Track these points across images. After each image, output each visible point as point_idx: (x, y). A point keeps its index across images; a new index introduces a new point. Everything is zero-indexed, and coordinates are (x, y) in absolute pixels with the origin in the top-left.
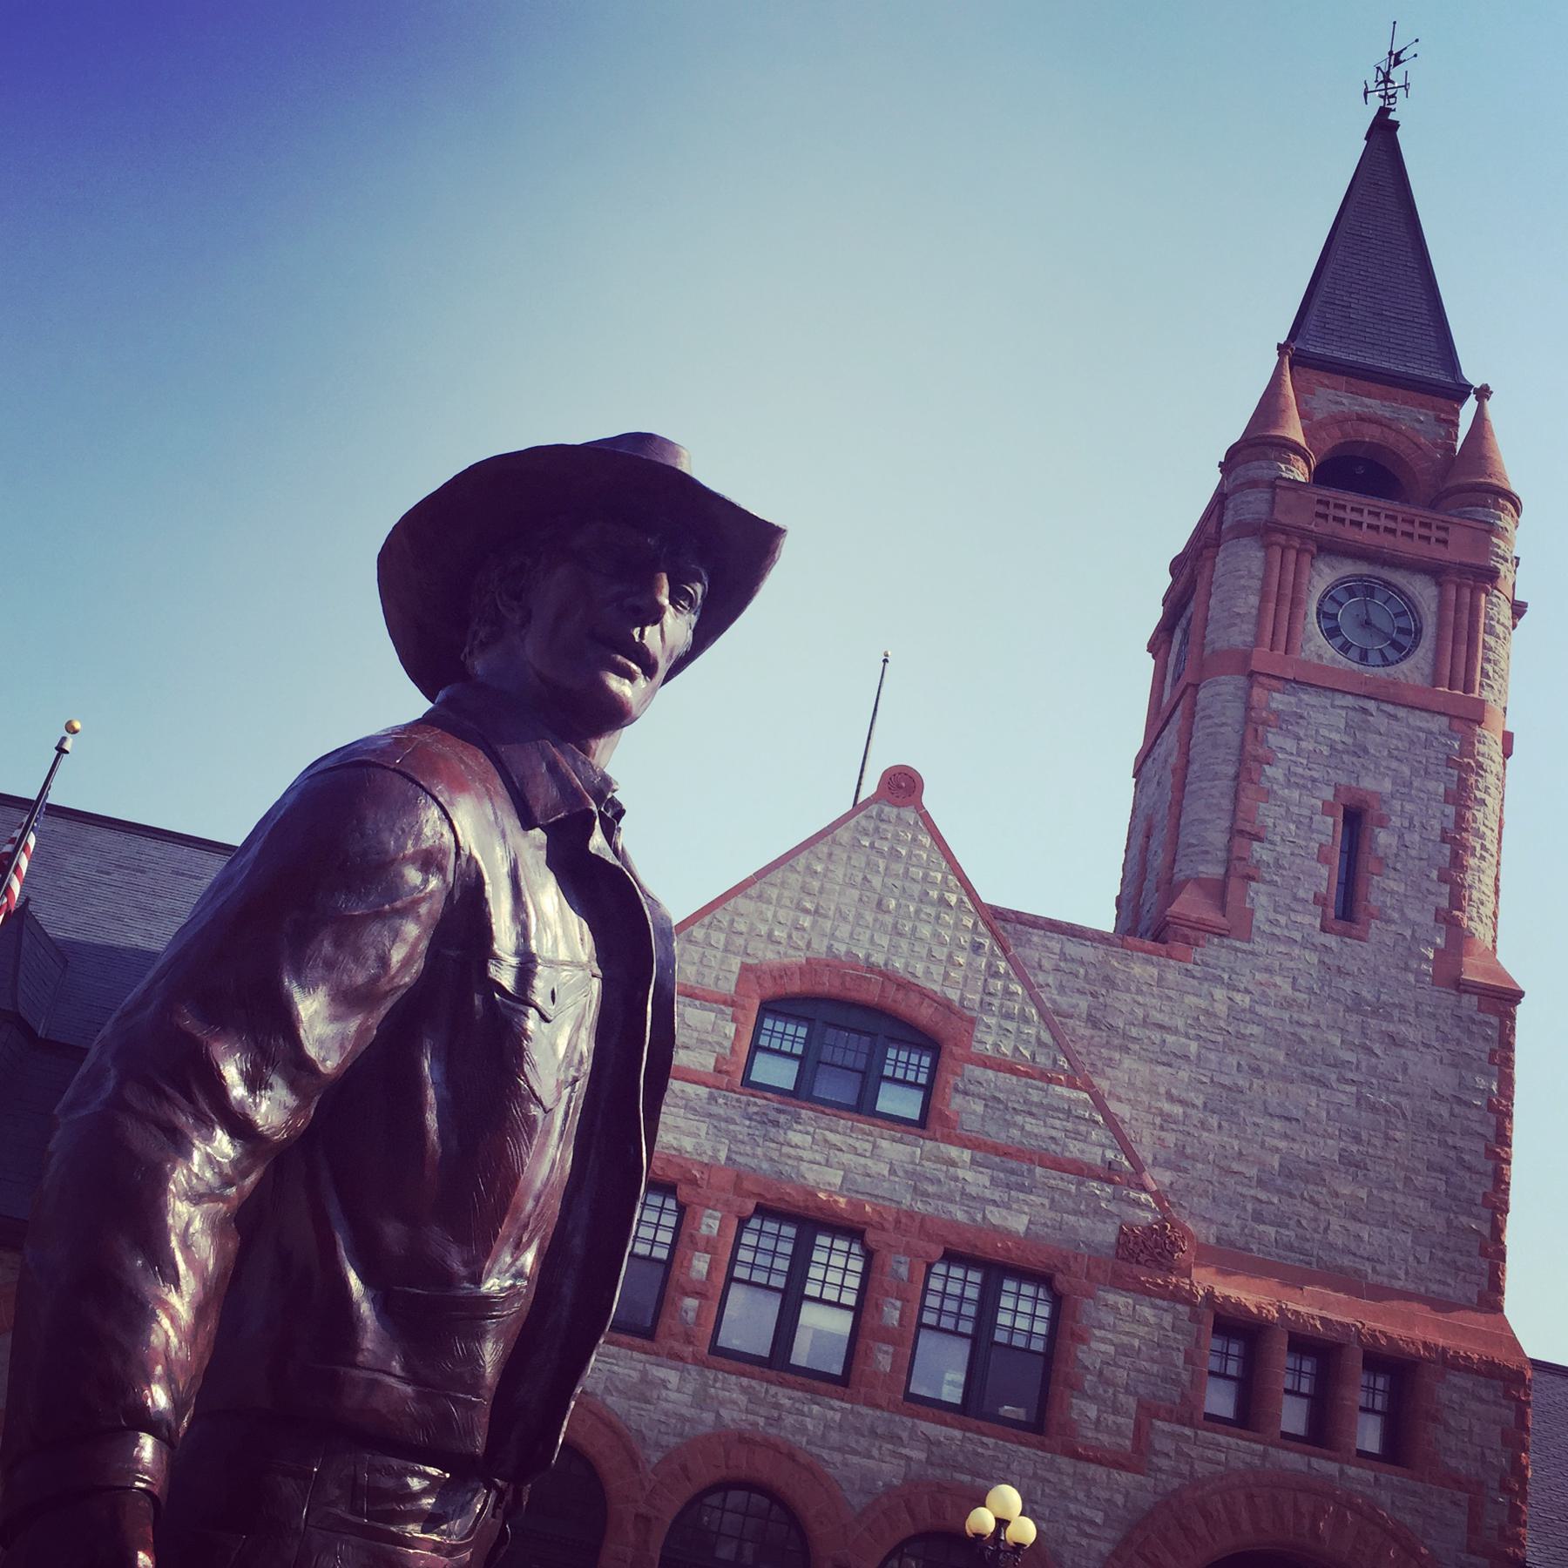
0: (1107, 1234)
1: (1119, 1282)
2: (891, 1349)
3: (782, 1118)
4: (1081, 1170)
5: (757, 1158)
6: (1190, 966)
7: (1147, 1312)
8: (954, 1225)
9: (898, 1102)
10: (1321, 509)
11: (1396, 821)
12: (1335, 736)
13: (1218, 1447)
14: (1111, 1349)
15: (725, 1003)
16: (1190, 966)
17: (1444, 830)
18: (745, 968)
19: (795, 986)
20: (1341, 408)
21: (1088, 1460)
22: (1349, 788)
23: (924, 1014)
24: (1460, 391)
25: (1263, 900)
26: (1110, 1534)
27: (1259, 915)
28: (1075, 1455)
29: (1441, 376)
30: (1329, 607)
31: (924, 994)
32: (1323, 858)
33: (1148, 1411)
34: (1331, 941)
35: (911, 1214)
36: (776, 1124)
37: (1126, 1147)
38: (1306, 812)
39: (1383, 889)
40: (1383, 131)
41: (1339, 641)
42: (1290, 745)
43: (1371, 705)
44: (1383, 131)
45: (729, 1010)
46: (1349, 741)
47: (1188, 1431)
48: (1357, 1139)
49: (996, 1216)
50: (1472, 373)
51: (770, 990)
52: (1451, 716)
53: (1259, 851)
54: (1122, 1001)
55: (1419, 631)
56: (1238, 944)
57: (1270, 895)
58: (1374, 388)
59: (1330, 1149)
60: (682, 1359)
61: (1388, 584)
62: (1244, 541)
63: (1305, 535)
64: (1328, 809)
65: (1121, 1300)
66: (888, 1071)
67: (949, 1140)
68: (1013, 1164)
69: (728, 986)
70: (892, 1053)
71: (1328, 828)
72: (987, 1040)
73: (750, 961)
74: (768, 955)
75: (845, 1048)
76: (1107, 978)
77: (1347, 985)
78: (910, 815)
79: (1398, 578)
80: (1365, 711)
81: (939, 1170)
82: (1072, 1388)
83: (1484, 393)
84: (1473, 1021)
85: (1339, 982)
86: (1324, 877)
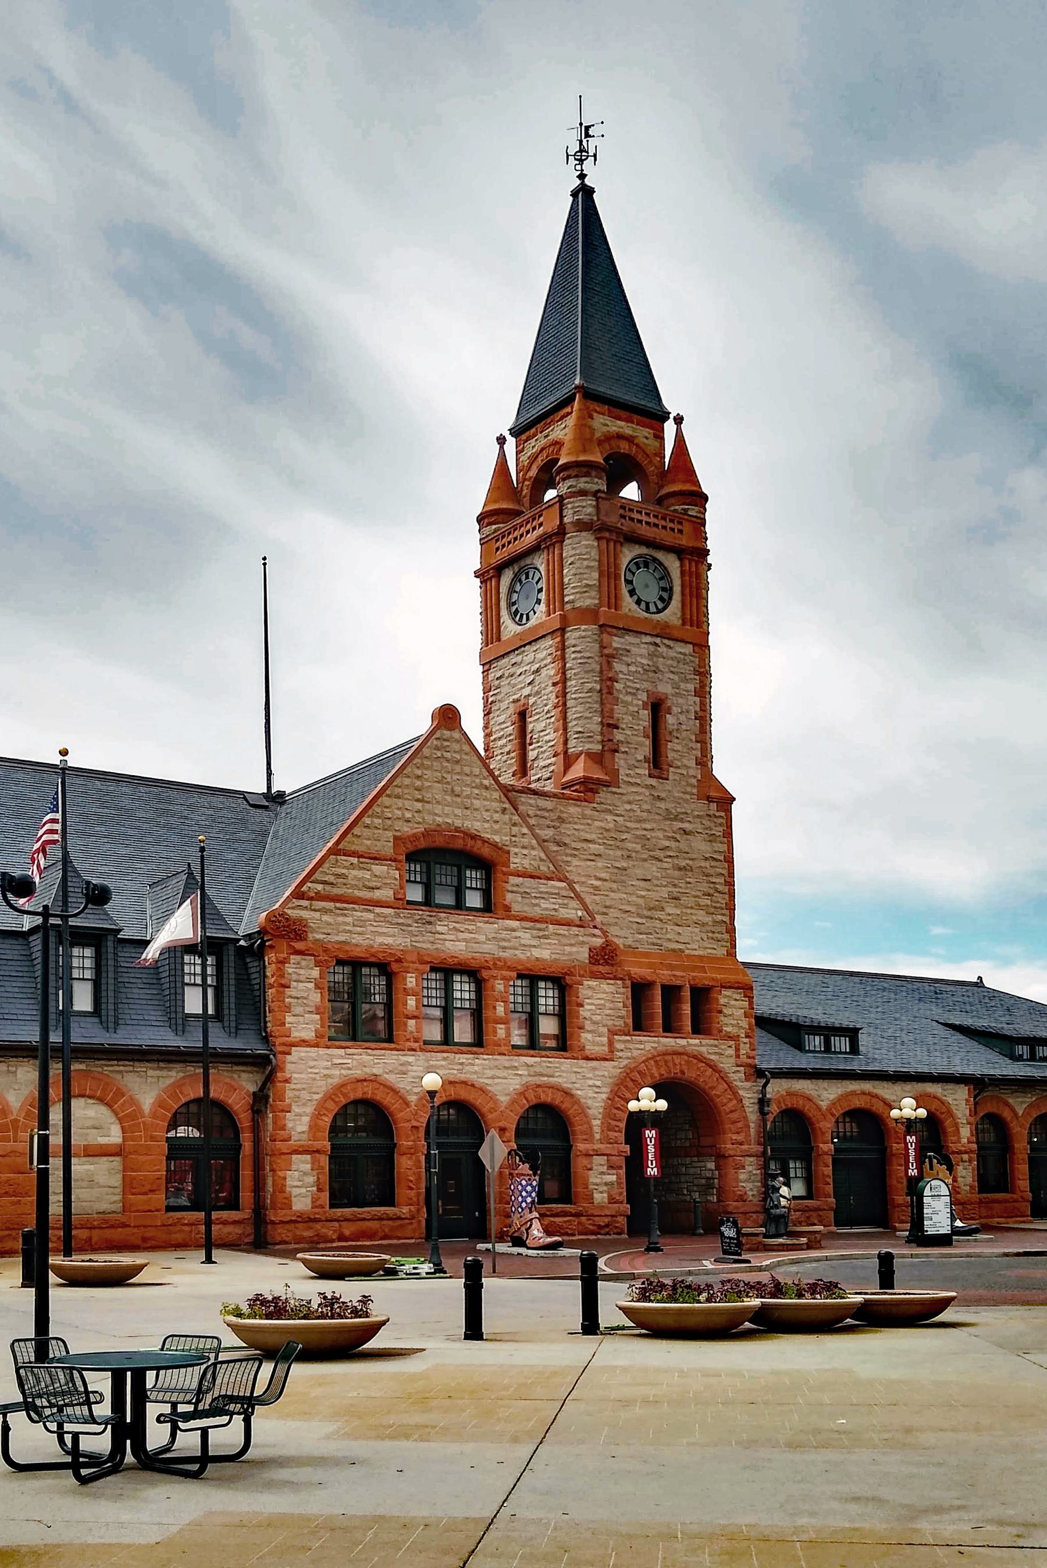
0: (584, 955)
1: (594, 976)
2: (503, 1026)
3: (432, 919)
4: (568, 923)
5: (424, 944)
6: (595, 805)
7: (604, 987)
8: (519, 961)
9: (473, 900)
10: (622, 511)
11: (675, 710)
12: (645, 661)
13: (641, 1042)
14: (593, 1007)
15: (390, 860)
16: (595, 805)
17: (696, 712)
18: (396, 838)
19: (422, 844)
20: (608, 429)
21: (592, 1059)
22: (653, 693)
23: (486, 851)
24: (664, 416)
25: (622, 763)
26: (604, 1090)
27: (621, 772)
28: (587, 1059)
29: (651, 405)
30: (629, 577)
31: (485, 841)
32: (646, 736)
33: (612, 1033)
34: (653, 782)
35: (499, 959)
36: (430, 923)
37: (586, 908)
38: (636, 709)
39: (673, 750)
40: (584, 194)
41: (635, 597)
42: (624, 669)
43: (658, 640)
44: (584, 194)
45: (393, 864)
46: (650, 663)
47: (628, 1038)
48: (675, 886)
49: (537, 953)
50: (671, 402)
51: (411, 848)
52: (694, 645)
53: (618, 735)
54: (567, 829)
55: (671, 588)
56: (614, 790)
57: (625, 760)
58: (624, 414)
59: (664, 893)
60: (414, 1050)
61: (655, 560)
62: (584, 534)
63: (618, 531)
64: (645, 704)
65: (593, 983)
66: (468, 885)
67: (509, 918)
68: (538, 925)
69: (388, 849)
70: (468, 873)
71: (646, 714)
72: (517, 862)
73: (398, 834)
74: (407, 829)
75: (444, 875)
76: (559, 818)
77: (662, 805)
78: (456, 735)
79: (660, 556)
80: (656, 645)
81: (504, 934)
82: (580, 1028)
83: (679, 420)
84: (716, 817)
85: (659, 804)
86: (645, 749)
